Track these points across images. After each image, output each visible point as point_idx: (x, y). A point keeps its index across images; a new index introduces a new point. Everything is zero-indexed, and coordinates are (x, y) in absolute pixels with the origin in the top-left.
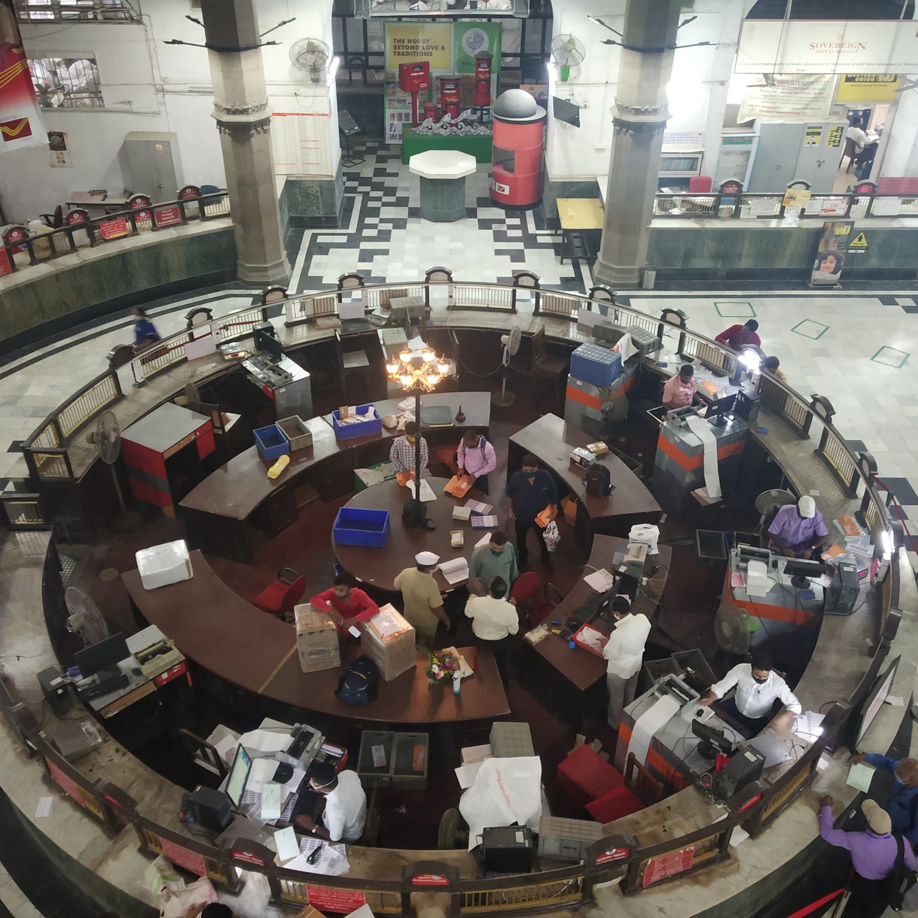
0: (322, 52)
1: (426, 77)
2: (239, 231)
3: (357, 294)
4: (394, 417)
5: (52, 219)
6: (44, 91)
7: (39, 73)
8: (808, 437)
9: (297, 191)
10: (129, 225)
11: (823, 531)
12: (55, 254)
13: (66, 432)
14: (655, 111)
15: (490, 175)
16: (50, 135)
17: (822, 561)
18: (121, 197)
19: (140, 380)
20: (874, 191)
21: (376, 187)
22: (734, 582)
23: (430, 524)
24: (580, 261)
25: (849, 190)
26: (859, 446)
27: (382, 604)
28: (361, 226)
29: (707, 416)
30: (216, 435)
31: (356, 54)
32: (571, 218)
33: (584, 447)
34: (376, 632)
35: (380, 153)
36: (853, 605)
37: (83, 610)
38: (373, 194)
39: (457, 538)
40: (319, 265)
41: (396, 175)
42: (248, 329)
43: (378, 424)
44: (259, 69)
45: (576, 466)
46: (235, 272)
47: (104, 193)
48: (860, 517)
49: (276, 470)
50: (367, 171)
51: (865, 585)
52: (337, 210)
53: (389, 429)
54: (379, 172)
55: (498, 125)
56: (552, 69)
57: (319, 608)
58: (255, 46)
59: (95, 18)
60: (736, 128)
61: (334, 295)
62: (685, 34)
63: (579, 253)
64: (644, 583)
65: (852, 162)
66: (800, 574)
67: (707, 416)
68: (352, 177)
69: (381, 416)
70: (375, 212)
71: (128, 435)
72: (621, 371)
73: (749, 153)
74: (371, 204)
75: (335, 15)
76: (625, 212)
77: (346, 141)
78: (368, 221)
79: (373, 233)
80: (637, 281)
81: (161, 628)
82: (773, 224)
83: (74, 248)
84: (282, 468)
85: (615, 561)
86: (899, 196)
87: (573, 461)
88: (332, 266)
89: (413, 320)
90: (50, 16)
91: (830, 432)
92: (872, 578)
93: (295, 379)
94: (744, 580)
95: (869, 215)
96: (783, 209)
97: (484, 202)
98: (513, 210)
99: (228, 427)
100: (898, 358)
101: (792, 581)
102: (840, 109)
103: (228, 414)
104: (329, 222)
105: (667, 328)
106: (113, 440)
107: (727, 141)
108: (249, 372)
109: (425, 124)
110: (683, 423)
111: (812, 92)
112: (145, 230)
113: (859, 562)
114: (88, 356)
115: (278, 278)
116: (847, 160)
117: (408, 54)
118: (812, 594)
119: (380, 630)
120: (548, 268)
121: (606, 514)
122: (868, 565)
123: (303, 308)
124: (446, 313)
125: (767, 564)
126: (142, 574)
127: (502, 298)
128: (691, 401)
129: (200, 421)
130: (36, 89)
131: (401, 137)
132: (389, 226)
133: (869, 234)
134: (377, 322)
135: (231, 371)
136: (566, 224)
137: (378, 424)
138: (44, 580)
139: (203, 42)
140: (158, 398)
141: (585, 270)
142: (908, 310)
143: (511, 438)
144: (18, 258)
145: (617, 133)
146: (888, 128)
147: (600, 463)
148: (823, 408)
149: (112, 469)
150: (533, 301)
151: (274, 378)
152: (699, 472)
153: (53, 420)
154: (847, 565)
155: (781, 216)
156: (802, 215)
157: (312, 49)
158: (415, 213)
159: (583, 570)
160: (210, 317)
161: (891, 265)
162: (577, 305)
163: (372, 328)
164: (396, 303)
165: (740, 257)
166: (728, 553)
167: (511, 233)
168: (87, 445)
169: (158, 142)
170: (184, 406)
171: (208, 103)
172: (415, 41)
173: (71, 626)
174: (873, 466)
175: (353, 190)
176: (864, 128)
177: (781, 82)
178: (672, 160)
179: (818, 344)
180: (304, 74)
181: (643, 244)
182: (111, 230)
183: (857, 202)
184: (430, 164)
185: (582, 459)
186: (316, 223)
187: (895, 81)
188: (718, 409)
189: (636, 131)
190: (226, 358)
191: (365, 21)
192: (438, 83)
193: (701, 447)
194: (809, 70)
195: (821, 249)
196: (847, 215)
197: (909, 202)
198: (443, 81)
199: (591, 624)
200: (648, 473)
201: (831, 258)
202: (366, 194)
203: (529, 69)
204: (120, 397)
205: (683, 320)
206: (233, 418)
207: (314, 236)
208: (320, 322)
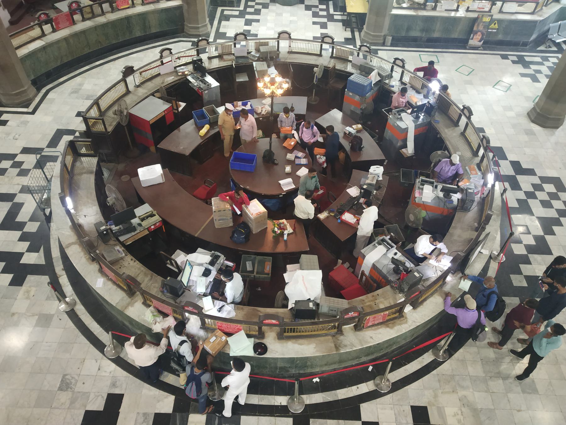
2: (185, 7)
4: (260, 108)
8: (459, 126)
11: (461, 171)
12: (94, 16)
13: (103, 109)
17: (458, 186)
19: (137, 84)
22: (417, 195)
23: (276, 162)
24: (355, 30)
27: (251, 199)
28: (246, 6)
30: (174, 113)
32: (352, 6)
33: (351, 126)
34: (249, 211)
37: (114, 196)
42: (189, 60)
45: (347, 135)
46: (183, 29)
51: (477, 198)
57: (223, 200)
63: (354, 25)
64: (374, 193)
66: (447, 192)
69: (254, 107)
79: (251, 10)
80: (382, 42)
82: (453, 14)
83: (103, 13)
84: (206, 131)
86: (517, 2)
87: (345, 133)
88: (232, 27)
89: (271, 58)
93: (212, 86)
94: (421, 194)
96: (458, 6)
99: (180, 109)
100: (506, 87)
101: (444, 195)
103: (180, 103)
110: (399, 117)
112: (138, 4)
113: (476, 187)
118: (452, 201)
120: (338, 32)
121: (359, 160)
122: (480, 189)
124: (287, 55)
125: (433, 186)
127: (315, 47)
128: (404, 105)
129: (167, 106)
132: (260, 7)
133: (500, 21)
136: (349, 10)
140: (146, 93)
141: (357, 34)
142: (514, 62)
147: (359, 135)
148: (468, 111)
151: (202, 86)
154: (470, 189)
155: (457, 10)
156: (468, 10)
160: (171, 53)
161: (508, 38)
163: (251, 61)
164: (263, 49)
165: (434, 31)
166: (415, 181)
167: (321, 13)
170: (159, 98)
179: (468, 78)
181: (387, 22)
185: (350, 132)
188: (416, 110)
190: (179, 74)
195: (475, 29)
199: (348, 211)
200: (380, 140)
201: (479, 33)
204: (128, 92)
205: (404, 64)
206: (183, 105)
207: (223, 11)
208: (225, 57)
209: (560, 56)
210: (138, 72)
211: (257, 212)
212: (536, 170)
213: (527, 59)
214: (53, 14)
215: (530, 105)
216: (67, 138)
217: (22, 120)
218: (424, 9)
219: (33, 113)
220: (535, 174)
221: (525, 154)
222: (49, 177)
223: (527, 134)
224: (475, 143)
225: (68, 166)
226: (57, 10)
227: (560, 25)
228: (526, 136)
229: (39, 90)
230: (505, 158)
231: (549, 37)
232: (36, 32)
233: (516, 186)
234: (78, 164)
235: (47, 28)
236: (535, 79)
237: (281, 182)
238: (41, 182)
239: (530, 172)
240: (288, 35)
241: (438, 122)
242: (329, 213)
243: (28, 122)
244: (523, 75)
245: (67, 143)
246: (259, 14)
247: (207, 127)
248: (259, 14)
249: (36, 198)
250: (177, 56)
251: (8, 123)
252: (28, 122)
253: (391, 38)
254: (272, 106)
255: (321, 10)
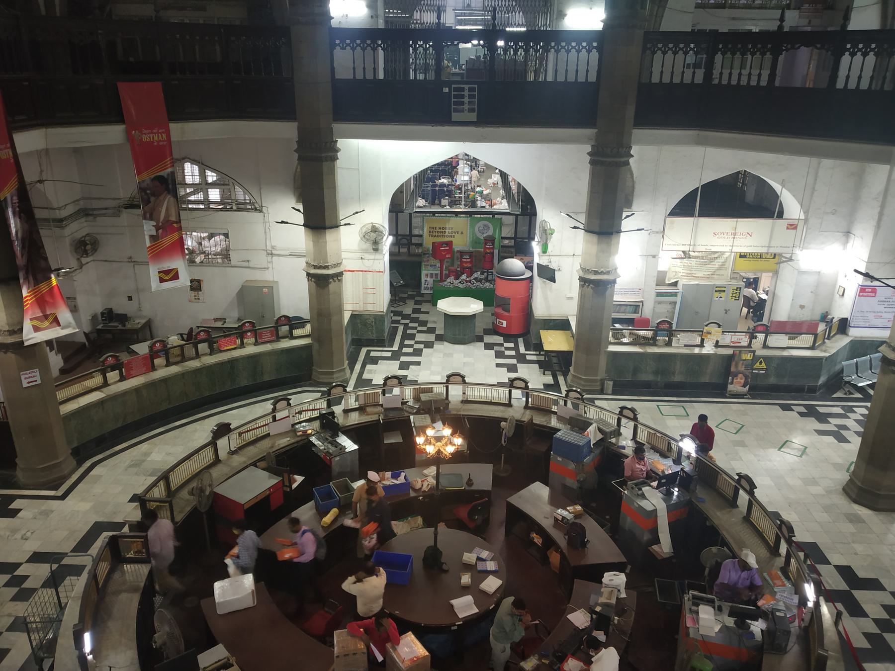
0: (381, 232)
1: (451, 251)
2: (316, 346)
3: (396, 391)
4: (419, 481)
5: (185, 337)
6: (192, 252)
7: (189, 243)
8: (737, 507)
9: (358, 321)
10: (238, 341)
11: (758, 582)
12: (183, 359)
13: (173, 487)
14: (608, 273)
15: (493, 315)
16: (192, 281)
17: (758, 607)
18: (235, 323)
19: (233, 449)
20: (767, 330)
21: (413, 320)
22: (689, 624)
23: (445, 567)
24: (558, 373)
25: (749, 329)
26: (775, 516)
27: (402, 632)
28: (402, 345)
29: (657, 488)
30: (285, 492)
31: (404, 236)
32: (550, 343)
33: (565, 508)
34: (399, 656)
35: (417, 298)
36: (786, 645)
37: (167, 628)
38: (411, 325)
39: (466, 579)
40: (370, 372)
41: (428, 313)
42: (316, 414)
43: (407, 485)
44: (338, 240)
45: (559, 523)
46: (311, 375)
47: (224, 320)
48: (785, 570)
49: (328, 519)
50: (408, 310)
51: (795, 627)
52: (386, 335)
53: (415, 490)
54: (415, 311)
55: (498, 281)
56: (536, 246)
57: (353, 634)
58: (336, 226)
59: (232, 208)
60: (665, 287)
61: (380, 391)
62: (626, 224)
63: (556, 367)
64: (616, 622)
65: (749, 312)
66: (742, 618)
67: (657, 488)
68: (396, 313)
69: (410, 479)
70: (412, 337)
71: (219, 490)
72: (591, 451)
73: (675, 303)
74: (409, 331)
75: (391, 211)
76: (590, 333)
77: (394, 289)
78: (407, 342)
79: (410, 350)
80: (599, 388)
81: (227, 647)
82: (697, 351)
83: (198, 356)
84: (332, 518)
85: (592, 602)
86: (786, 334)
87: (556, 519)
88: (378, 373)
89: (437, 409)
90: (202, 206)
91: (754, 502)
92: (799, 623)
93: (347, 450)
94: (696, 620)
95: (765, 346)
96: (702, 340)
97: (488, 332)
98: (508, 337)
99: (295, 486)
100: (799, 450)
101: (735, 623)
102: (735, 275)
103: (296, 476)
104: (380, 343)
105: (624, 421)
106: (207, 493)
107: (659, 294)
108: (314, 445)
109: (448, 280)
110: (640, 492)
111: (717, 264)
112: (250, 344)
113: (788, 607)
114: (199, 431)
115: (341, 379)
116: (745, 310)
117: (438, 236)
118: (752, 635)
119: (401, 654)
120: (536, 378)
121: (583, 563)
122: (795, 611)
123: (357, 400)
124: (460, 405)
125: (714, 608)
126: (217, 601)
127: (501, 394)
128: (645, 475)
129: (274, 481)
130: (187, 252)
131: (432, 288)
132: (422, 346)
133: (767, 359)
134: (410, 410)
135: (301, 443)
136: (547, 347)
137: (407, 485)
138: (140, 603)
139: (302, 222)
140: (245, 462)
141: (561, 379)
142: (802, 414)
143: (509, 500)
144: (157, 361)
145: (582, 286)
146: (772, 289)
147: (578, 521)
148: (747, 483)
149: (205, 516)
150: (524, 399)
151: (332, 449)
152: (655, 531)
153: (165, 477)
154: (779, 611)
155: (702, 345)
156: (717, 345)
157: (374, 229)
158: (440, 338)
159: (565, 610)
160: (289, 404)
161: (785, 382)
162: (556, 403)
163: (406, 414)
164: (424, 397)
165: (674, 374)
166: (682, 598)
167: (507, 353)
168: (187, 497)
169: (265, 287)
170: (263, 469)
171: (302, 263)
172: (443, 228)
173: (155, 642)
174: (791, 530)
175: (398, 322)
176: (755, 289)
177: (695, 257)
178: (621, 306)
179: (737, 437)
180: (368, 246)
181: (603, 363)
182: (226, 344)
183: (756, 337)
184: (449, 305)
185: (563, 518)
186: (370, 343)
187: (774, 258)
188: (666, 482)
189: (595, 285)
190: (299, 434)
191: (410, 214)
192: (458, 254)
193: (655, 511)
194: (714, 249)
195: (733, 369)
196: (750, 345)
197: (793, 339)
198: (462, 253)
199: (574, 655)
200: (615, 531)
201: (740, 375)
202: (406, 325)
203: (521, 248)
204: (217, 461)
205: (635, 415)
206: (299, 479)
207: (368, 352)
208: (369, 409)
209: (869, 404)
210: (235, 432)
211: (411, 656)
212: (882, 581)
213: (822, 410)
214: (124, 357)
215: (845, 477)
216: (106, 535)
217: (43, 508)
218: (654, 344)
219: (63, 497)
220: (883, 589)
221: (856, 554)
222: (63, 601)
223: (851, 521)
224: (770, 534)
225: (99, 579)
226: (133, 352)
227: (857, 363)
228: (850, 525)
229: (80, 463)
230: (827, 562)
231: (847, 379)
232: (98, 380)
233: (856, 610)
234: (117, 576)
235: (113, 376)
236: (842, 439)
237: (454, 602)
238: (49, 610)
239: (873, 585)
240: (460, 379)
241: (703, 501)
242: (540, 660)
243: (52, 511)
244: (821, 433)
245: (107, 540)
246: (420, 355)
247: (334, 511)
248: (420, 355)
249: (33, 638)
250: (297, 409)
251: (20, 515)
252: (52, 511)
253: (611, 383)
254: (437, 477)
255: (507, 349)
